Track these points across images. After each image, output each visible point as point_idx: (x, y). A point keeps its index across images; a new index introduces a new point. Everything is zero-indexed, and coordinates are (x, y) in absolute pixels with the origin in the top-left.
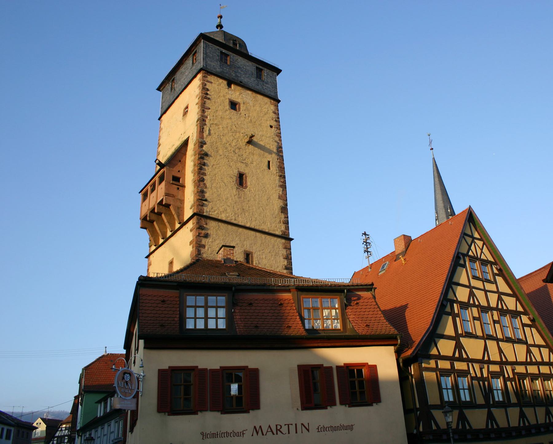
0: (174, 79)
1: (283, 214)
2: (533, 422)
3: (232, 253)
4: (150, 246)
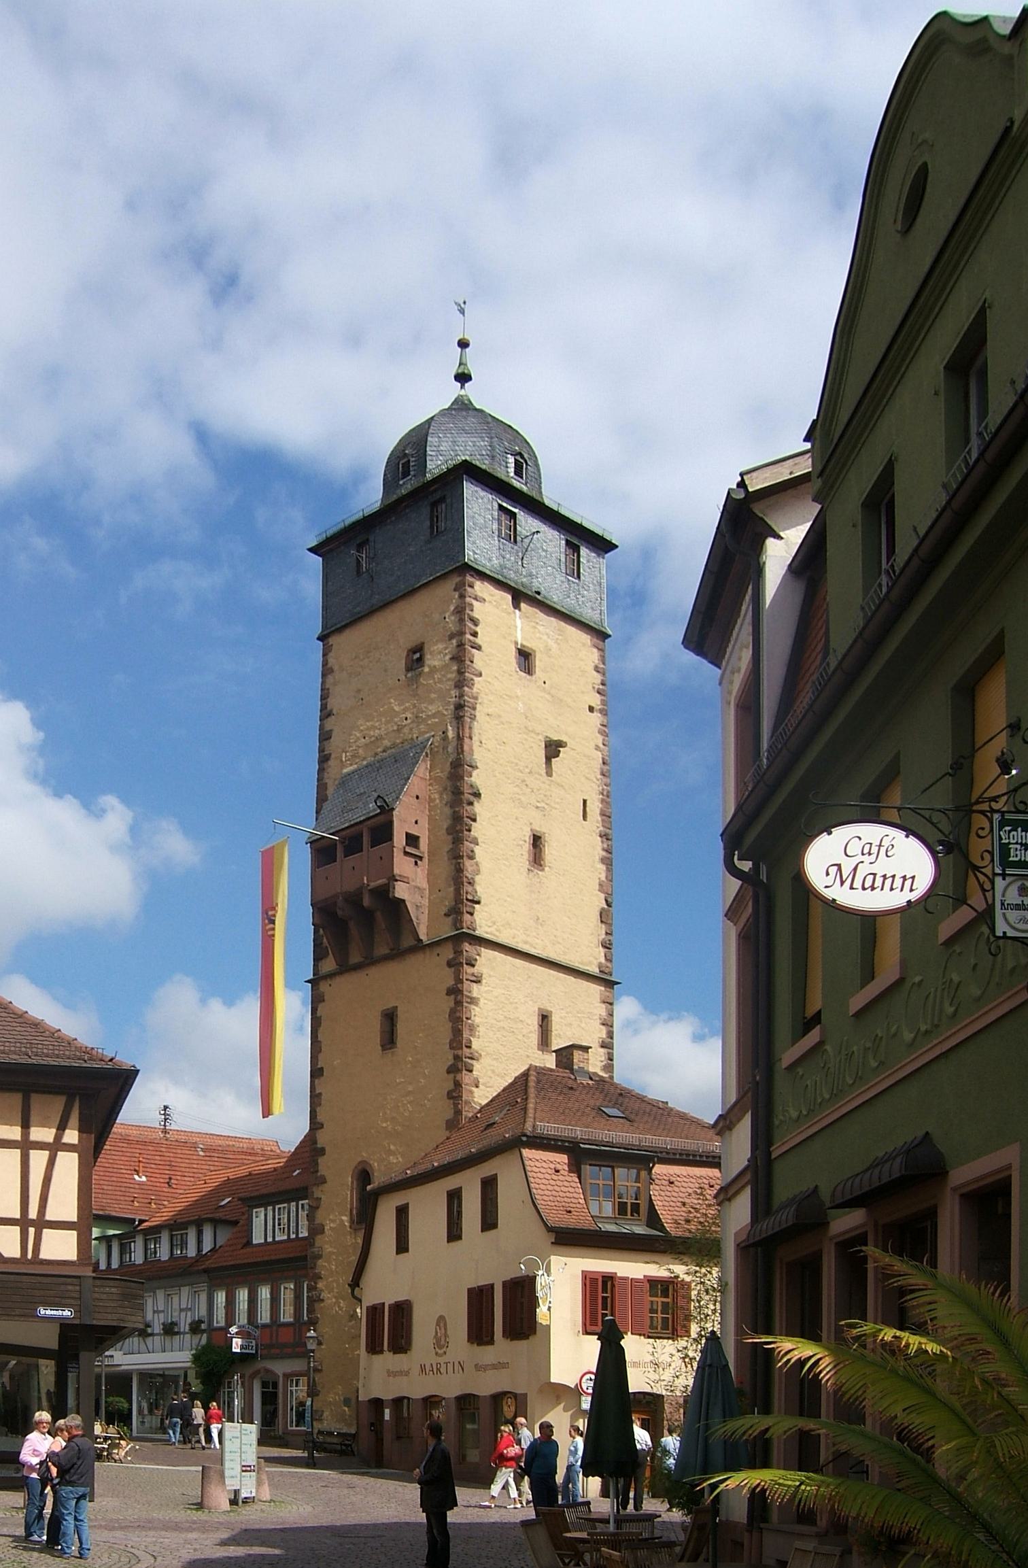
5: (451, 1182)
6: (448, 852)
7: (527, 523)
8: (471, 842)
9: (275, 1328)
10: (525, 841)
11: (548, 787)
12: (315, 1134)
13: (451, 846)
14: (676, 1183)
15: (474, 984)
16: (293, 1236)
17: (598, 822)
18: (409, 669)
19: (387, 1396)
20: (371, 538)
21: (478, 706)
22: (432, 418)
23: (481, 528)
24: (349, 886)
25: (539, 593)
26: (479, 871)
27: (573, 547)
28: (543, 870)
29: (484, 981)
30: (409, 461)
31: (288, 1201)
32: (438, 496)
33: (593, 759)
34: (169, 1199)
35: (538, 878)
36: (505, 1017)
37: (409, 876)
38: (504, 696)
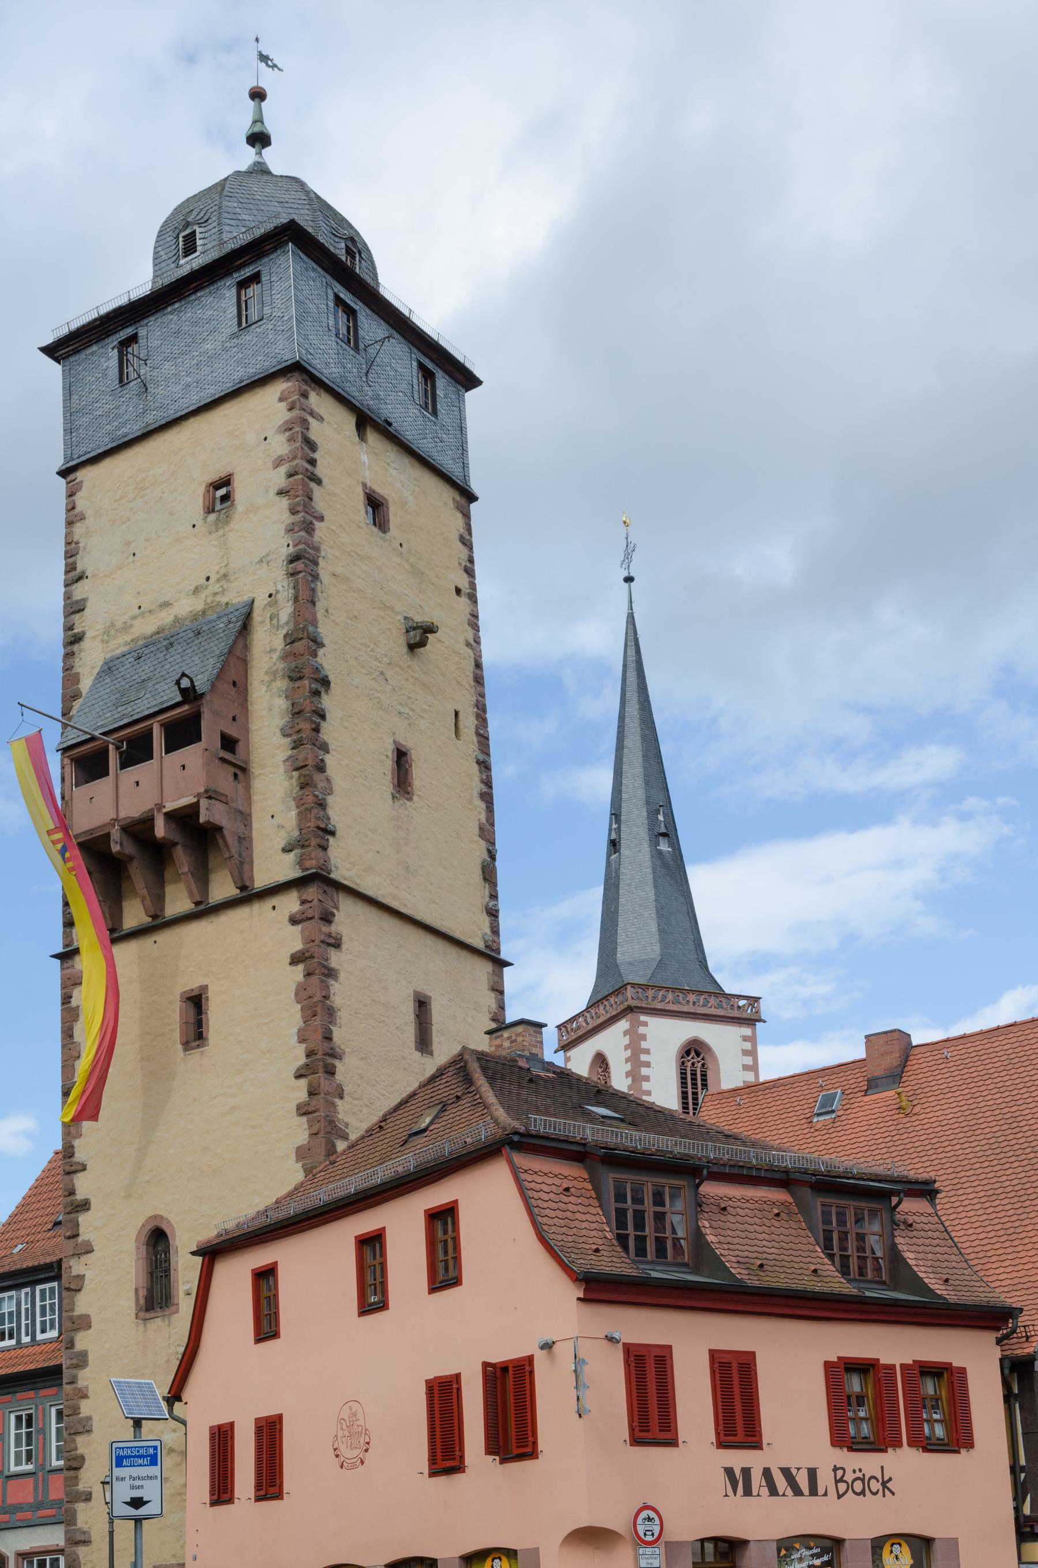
0: (134, 339)
1: (487, 886)
5: (364, 1223)
6: (284, 761)
7: (371, 327)
8: (319, 748)
10: (387, 756)
12: (72, 1181)
13: (290, 753)
15: (332, 949)
16: (26, 1339)
17: (473, 743)
18: (210, 510)
20: (142, 332)
21: (321, 561)
22: (226, 179)
24: (132, 809)
25: (390, 424)
26: (331, 789)
27: (428, 375)
28: (410, 799)
29: (344, 946)
30: (194, 232)
31: (18, 1287)
32: (248, 272)
36: (373, 1000)
37: (227, 793)
38: (353, 554)
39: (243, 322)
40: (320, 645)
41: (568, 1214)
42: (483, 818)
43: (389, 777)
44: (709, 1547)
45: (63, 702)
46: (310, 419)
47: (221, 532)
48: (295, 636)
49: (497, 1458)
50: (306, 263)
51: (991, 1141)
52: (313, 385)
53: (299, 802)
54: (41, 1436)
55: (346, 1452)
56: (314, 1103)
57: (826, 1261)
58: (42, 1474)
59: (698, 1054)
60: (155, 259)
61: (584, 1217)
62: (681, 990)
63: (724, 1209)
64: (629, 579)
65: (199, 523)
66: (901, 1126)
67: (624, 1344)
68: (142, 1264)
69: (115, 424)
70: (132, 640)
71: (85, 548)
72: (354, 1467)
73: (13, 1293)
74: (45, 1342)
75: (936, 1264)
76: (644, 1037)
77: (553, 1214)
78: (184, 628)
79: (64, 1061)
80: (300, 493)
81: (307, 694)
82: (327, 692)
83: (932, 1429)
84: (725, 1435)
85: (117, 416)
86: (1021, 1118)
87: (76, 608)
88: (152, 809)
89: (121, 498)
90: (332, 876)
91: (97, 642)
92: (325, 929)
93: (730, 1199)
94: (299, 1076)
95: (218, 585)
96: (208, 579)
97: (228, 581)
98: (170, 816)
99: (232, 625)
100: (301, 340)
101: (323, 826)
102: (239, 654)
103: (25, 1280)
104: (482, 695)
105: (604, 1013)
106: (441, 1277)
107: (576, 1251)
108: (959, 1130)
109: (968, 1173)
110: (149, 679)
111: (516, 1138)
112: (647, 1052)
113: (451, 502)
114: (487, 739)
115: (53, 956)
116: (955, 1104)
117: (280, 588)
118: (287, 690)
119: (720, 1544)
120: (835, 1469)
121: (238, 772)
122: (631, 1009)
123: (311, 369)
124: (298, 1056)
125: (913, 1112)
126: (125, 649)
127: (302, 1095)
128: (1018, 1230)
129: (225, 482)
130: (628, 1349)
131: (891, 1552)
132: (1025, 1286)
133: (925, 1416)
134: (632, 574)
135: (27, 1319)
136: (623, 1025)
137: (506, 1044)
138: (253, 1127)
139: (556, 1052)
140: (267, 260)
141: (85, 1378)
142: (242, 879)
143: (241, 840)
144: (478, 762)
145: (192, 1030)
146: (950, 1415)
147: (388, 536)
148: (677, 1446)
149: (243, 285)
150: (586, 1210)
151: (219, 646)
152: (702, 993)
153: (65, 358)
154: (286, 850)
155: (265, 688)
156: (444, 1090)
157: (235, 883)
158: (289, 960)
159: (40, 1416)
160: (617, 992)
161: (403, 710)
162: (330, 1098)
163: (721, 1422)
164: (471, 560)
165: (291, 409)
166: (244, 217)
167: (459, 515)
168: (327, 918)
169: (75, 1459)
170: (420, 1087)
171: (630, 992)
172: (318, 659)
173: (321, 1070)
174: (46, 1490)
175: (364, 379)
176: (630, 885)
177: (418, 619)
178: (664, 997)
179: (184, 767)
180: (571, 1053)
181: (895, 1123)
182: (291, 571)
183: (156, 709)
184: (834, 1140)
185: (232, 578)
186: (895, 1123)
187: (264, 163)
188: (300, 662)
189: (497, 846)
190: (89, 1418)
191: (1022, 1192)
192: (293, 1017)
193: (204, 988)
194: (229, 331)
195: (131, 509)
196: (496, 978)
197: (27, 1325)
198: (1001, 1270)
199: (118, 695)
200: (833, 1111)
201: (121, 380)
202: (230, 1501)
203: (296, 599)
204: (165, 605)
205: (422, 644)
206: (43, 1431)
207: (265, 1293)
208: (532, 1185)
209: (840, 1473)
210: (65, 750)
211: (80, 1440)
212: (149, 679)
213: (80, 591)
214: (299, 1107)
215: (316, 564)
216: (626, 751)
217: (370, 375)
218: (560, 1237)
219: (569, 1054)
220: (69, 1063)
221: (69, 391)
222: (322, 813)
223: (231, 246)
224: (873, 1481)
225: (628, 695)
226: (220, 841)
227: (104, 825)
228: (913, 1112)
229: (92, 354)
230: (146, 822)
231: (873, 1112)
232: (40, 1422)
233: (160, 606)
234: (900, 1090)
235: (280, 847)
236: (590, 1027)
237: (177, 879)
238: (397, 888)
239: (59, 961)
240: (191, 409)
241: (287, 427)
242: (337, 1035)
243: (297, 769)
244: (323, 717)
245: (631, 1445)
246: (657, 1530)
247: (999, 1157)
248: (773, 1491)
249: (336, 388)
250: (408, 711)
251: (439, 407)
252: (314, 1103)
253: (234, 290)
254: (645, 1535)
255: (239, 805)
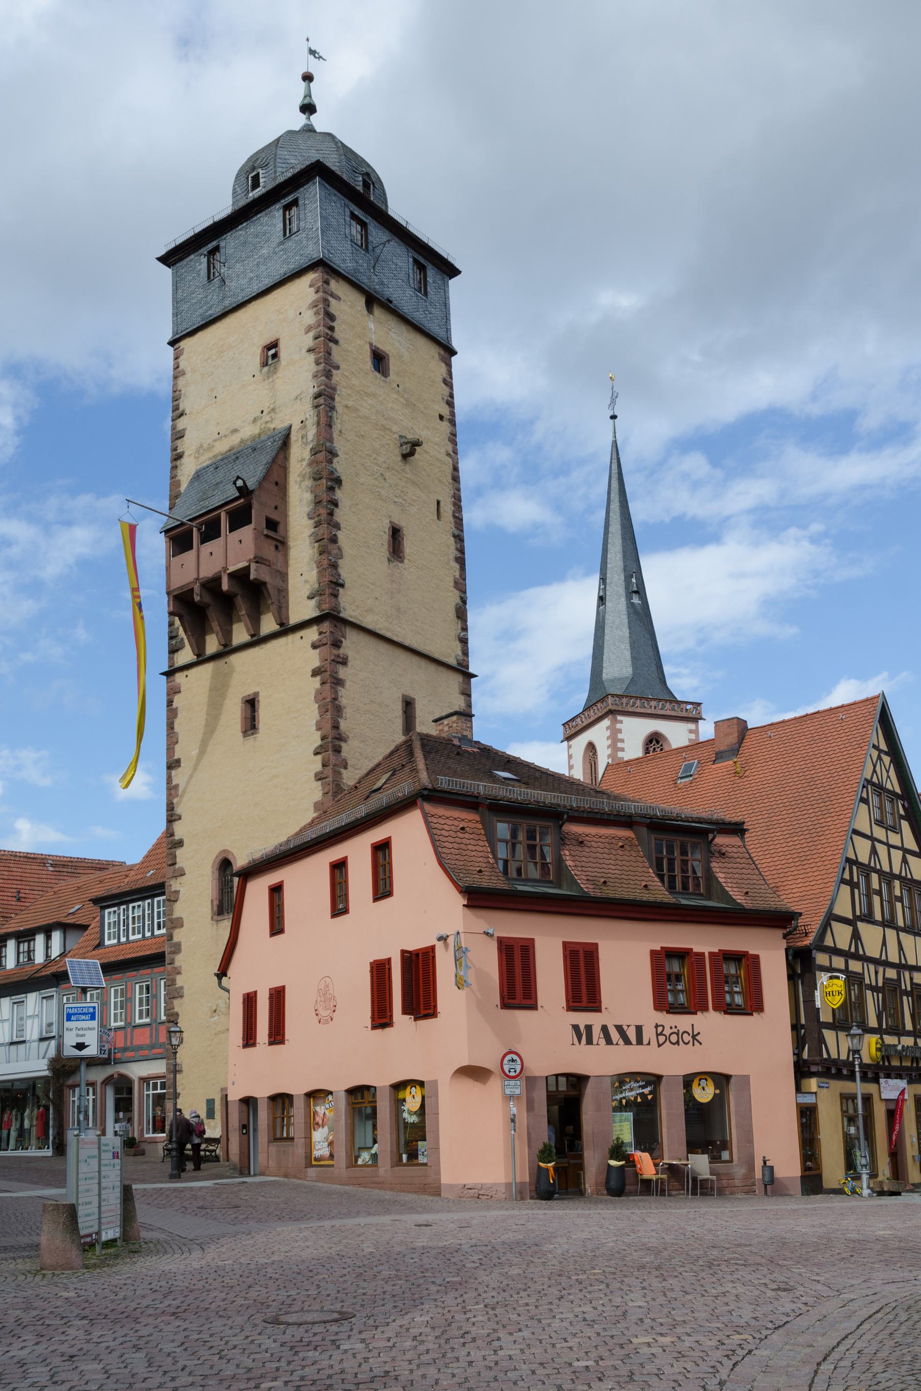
0: (217, 249)
2: (834, 1055)
3: (469, 727)
4: (173, 651)
6: (310, 536)
7: (377, 234)
8: (333, 527)
9: (129, 1030)
10: (385, 532)
11: (404, 484)
13: (313, 530)
14: (585, 842)
15: (341, 665)
16: (148, 934)
18: (265, 364)
19: (262, 1092)
20: (222, 244)
21: (336, 397)
23: (335, 230)
24: (207, 572)
25: (391, 302)
26: (342, 555)
27: (422, 268)
28: (402, 562)
29: (350, 664)
30: (258, 173)
32: (289, 199)
33: (445, 464)
34: (17, 912)
35: (398, 568)
36: (371, 701)
39: (287, 233)
40: (335, 455)
41: (462, 846)
42: (457, 574)
43: (386, 546)
44: (563, 1080)
45: (170, 500)
46: (330, 299)
47: (271, 380)
48: (317, 449)
49: (412, 1017)
50: (329, 190)
51: (795, 795)
52: (333, 275)
53: (319, 564)
54: (154, 1000)
55: (324, 1013)
56: (326, 772)
57: (656, 879)
58: (155, 1024)
59: (658, 742)
60: (234, 193)
61: (474, 848)
62: (646, 699)
63: (582, 842)
64: (614, 417)
65: (257, 374)
66: (736, 785)
67: (498, 937)
68: (216, 883)
69: (205, 308)
70: (214, 456)
71: (185, 395)
72: (327, 1022)
73: (140, 903)
74: (159, 936)
75: (740, 881)
76: (620, 731)
77: (450, 846)
78: (247, 446)
79: (168, 745)
80: (322, 350)
81: (325, 489)
82: (339, 488)
83: (733, 998)
84: (573, 1002)
85: (207, 303)
86: (817, 778)
87: (179, 435)
88: (220, 571)
89: (208, 359)
90: (341, 615)
91: (192, 459)
92: (335, 652)
93: (587, 835)
94: (316, 754)
95: (268, 416)
96: (262, 412)
97: (275, 413)
98: (232, 576)
99: (276, 443)
100: (324, 243)
101: (334, 580)
102: (280, 463)
103: (147, 894)
104: (459, 490)
105: (593, 714)
106: (381, 891)
107: (464, 872)
108: (774, 787)
109: (778, 818)
110: (222, 482)
111: (426, 793)
112: (622, 741)
113: (437, 356)
114: (462, 520)
115: (160, 674)
116: (773, 769)
117: (308, 416)
118: (312, 487)
119: (571, 1079)
120: (657, 1026)
121: (279, 544)
122: (611, 712)
123: (332, 264)
124: (315, 740)
125: (745, 775)
126: (208, 462)
127: (318, 767)
128: (809, 858)
129: (274, 345)
130: (501, 941)
131: (699, 1085)
132: (810, 897)
133: (727, 989)
134: (616, 414)
135: (149, 921)
136: (606, 723)
137: (446, 729)
138: (287, 789)
139: (562, 742)
140: (302, 189)
141: (180, 960)
142: (280, 618)
143: (279, 591)
144: (454, 536)
145: (249, 724)
146: (746, 988)
147: (388, 379)
148: (601, 1012)
149: (287, 208)
150: (476, 843)
151: (265, 458)
152: (660, 700)
153: (173, 265)
154: (310, 598)
155: (297, 486)
156: (396, 761)
157: (276, 621)
158: (311, 673)
159: (154, 986)
160: (602, 700)
161: (397, 500)
162: (337, 769)
163: (570, 993)
164: (452, 396)
165: (317, 292)
166: (292, 161)
167: (443, 365)
168: (337, 644)
169: (172, 1015)
170: (383, 759)
171: (610, 700)
172: (333, 465)
173: (330, 749)
174: (157, 1036)
175: (372, 271)
176: (612, 626)
177: (410, 437)
178: (634, 703)
179: (240, 541)
180: (573, 742)
181: (732, 783)
182: (315, 404)
183: (223, 502)
184: (690, 796)
185: (277, 411)
186: (732, 783)
187: (312, 125)
188: (321, 467)
189: (468, 594)
190: (182, 988)
191: (813, 831)
192: (311, 713)
193: (256, 694)
194: (278, 240)
195: (214, 366)
196: (465, 686)
197: (149, 924)
198: (795, 886)
199: (201, 494)
200: (691, 776)
201: (209, 277)
202: (254, 1045)
203: (318, 424)
204: (235, 431)
205: (412, 453)
206: (156, 996)
207: (276, 902)
208: (436, 826)
209: (660, 1029)
210: (167, 532)
211: (176, 1002)
212: (222, 482)
213: (181, 424)
214: (316, 775)
215: (333, 399)
216: (610, 535)
217: (377, 268)
218: (454, 862)
219: (571, 743)
220: (171, 746)
221: (176, 287)
222: (334, 571)
223: (281, 179)
224: (685, 1035)
225: (612, 496)
226: (264, 591)
227: (190, 583)
228: (745, 775)
229: (191, 260)
230: (217, 579)
231: (718, 775)
232: (154, 990)
233: (232, 432)
234: (735, 760)
235: (306, 596)
236: (584, 724)
237: (240, 621)
238: (391, 623)
239: (165, 677)
240: (253, 295)
241: (314, 305)
242: (343, 725)
243: (317, 542)
244: (336, 505)
245: (501, 1008)
246: (518, 1068)
247: (799, 806)
248: (609, 1041)
249: (350, 277)
250: (401, 500)
251: (429, 290)
252: (326, 772)
253: (281, 211)
254: (509, 1071)
255: (279, 567)
